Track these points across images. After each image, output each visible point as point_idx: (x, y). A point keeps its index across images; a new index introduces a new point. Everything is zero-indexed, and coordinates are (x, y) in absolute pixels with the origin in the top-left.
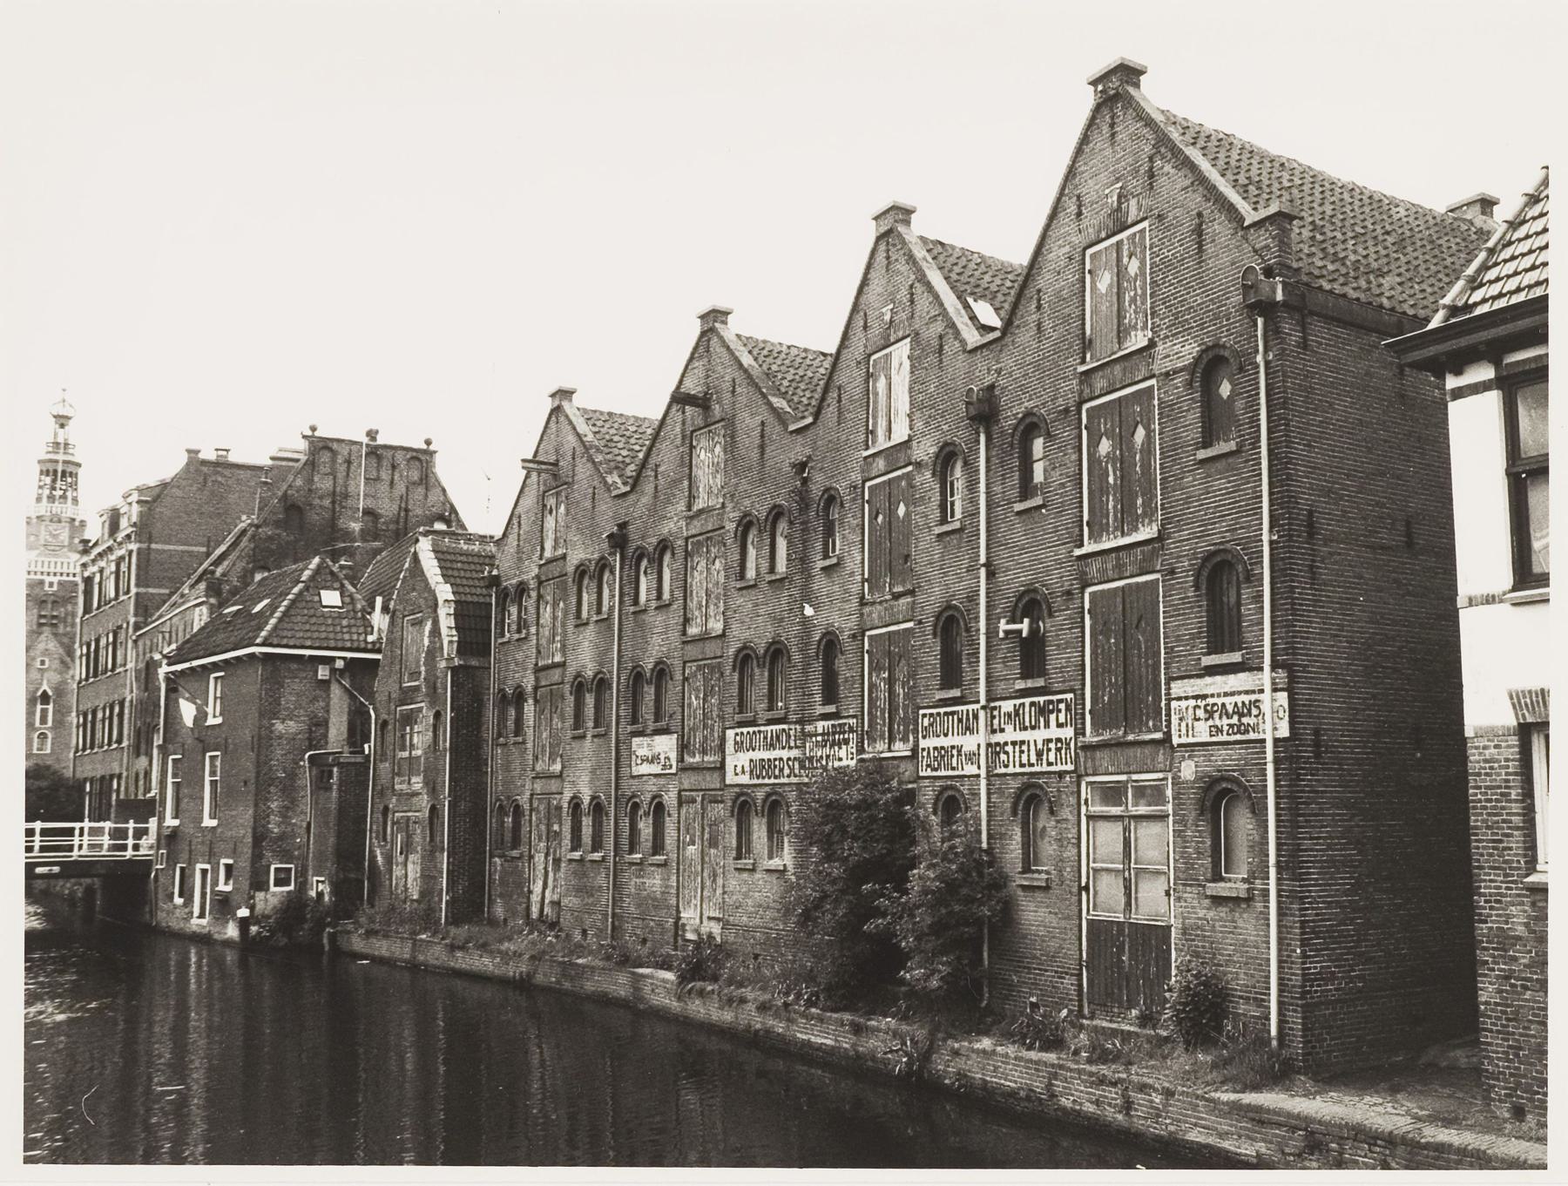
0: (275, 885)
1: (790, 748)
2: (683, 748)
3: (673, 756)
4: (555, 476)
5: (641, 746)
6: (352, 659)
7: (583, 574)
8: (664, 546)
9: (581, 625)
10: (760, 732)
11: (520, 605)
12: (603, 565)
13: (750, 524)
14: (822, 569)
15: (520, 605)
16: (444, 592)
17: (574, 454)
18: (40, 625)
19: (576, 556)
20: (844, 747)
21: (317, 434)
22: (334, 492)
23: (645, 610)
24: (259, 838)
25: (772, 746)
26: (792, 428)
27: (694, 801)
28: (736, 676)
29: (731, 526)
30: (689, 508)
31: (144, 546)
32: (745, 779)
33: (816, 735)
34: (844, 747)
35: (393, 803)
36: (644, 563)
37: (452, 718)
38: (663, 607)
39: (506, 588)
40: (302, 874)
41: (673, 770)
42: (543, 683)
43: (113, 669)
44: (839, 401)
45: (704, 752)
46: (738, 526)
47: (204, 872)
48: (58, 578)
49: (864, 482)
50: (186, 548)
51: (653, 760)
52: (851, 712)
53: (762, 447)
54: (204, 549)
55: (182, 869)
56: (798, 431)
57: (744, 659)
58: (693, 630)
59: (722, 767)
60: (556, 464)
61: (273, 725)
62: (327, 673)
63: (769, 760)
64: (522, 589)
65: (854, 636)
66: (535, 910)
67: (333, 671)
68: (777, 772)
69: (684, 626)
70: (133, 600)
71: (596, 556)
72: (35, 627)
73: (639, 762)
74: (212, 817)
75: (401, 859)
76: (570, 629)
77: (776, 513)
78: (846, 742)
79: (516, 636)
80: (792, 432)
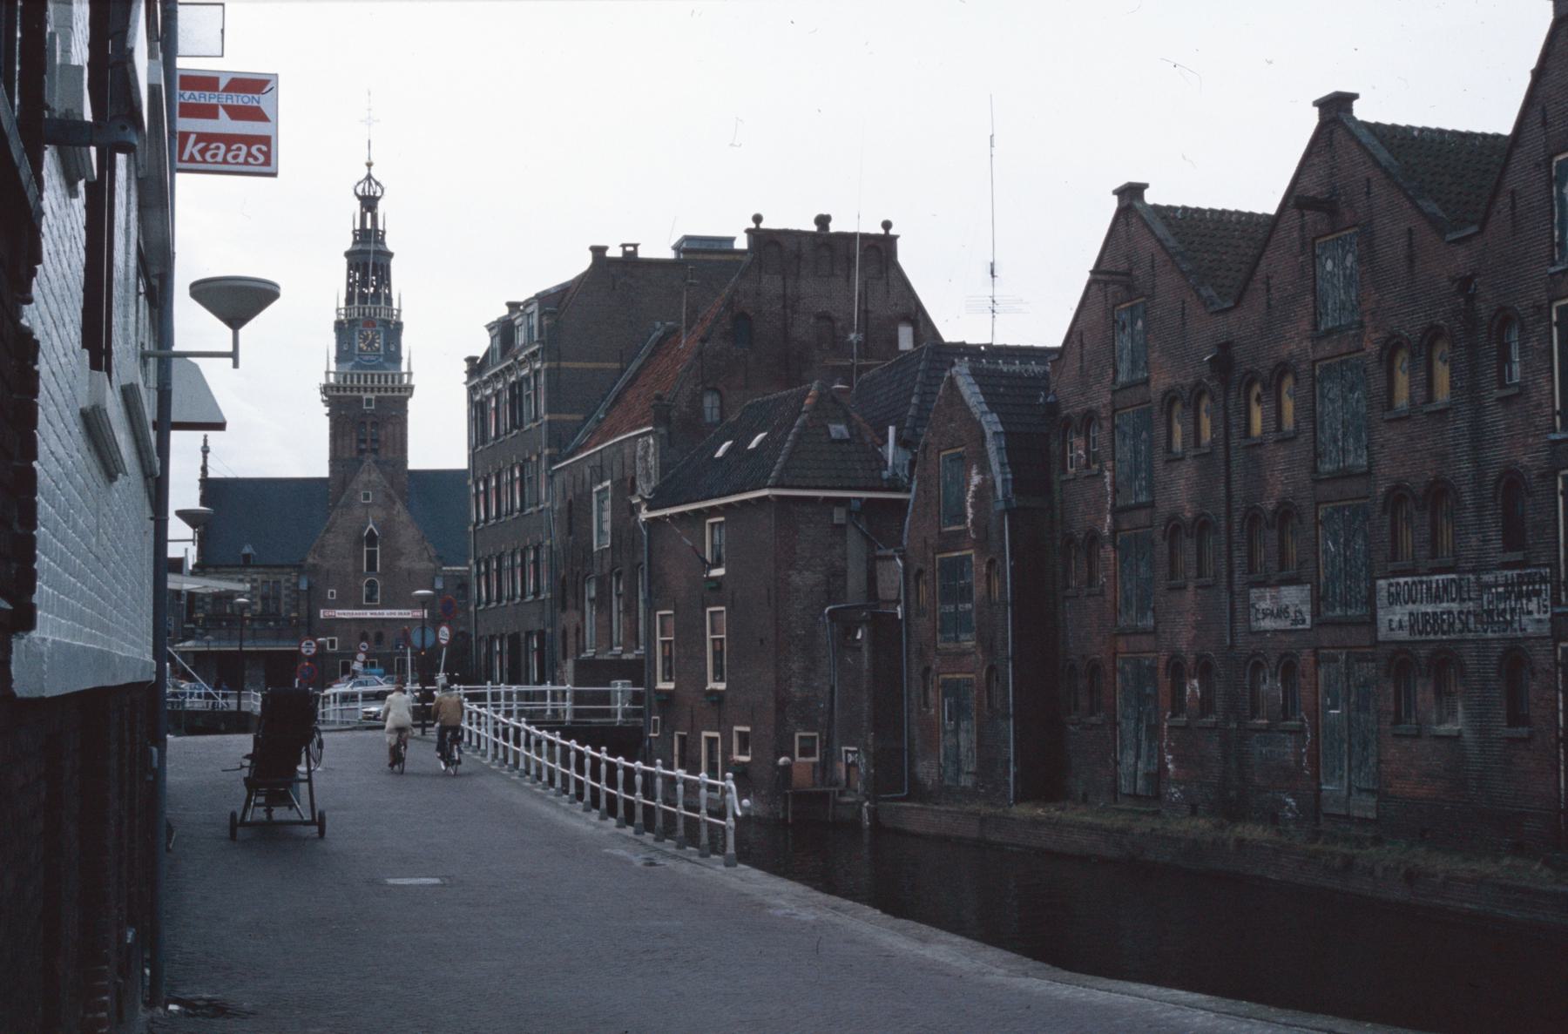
0: (801, 755)
1: (1463, 600)
2: (1317, 600)
3: (1306, 609)
4: (1129, 288)
5: (1264, 600)
6: (869, 500)
7: (1172, 402)
8: (1283, 369)
9: (1172, 459)
10: (1421, 582)
11: (1087, 436)
12: (1198, 392)
13: (1398, 346)
14: (1499, 399)
15: (1087, 436)
16: (991, 424)
17: (1153, 261)
18: (361, 451)
19: (1161, 382)
20: (1535, 600)
21: (763, 226)
22: (785, 295)
23: (1260, 445)
24: (782, 704)
25: (1437, 598)
26: (1449, 237)
27: (1336, 660)
28: (1387, 518)
29: (1372, 348)
30: (1315, 326)
31: (554, 364)
32: (1404, 635)
33: (1496, 586)
34: (1535, 600)
35: (936, 663)
36: (1257, 389)
37: (1011, 568)
38: (1285, 440)
39: (1068, 416)
40: (828, 745)
41: (1307, 626)
42: (1125, 526)
43: (522, 509)
44: (1513, 207)
45: (1347, 605)
46: (1382, 349)
47: (712, 741)
48: (376, 394)
49: (1551, 302)
50: (600, 365)
51: (1281, 613)
52: (1543, 560)
53: (1411, 259)
54: (617, 365)
55: (683, 739)
56: (1458, 241)
57: (1397, 496)
58: (1327, 467)
59: (1373, 621)
60: (1128, 274)
61: (789, 576)
62: (843, 515)
63: (1435, 613)
64: (1089, 418)
65: (1543, 476)
66: (1124, 783)
67: (849, 513)
68: (1445, 627)
69: (1315, 461)
70: (544, 429)
71: (1191, 380)
72: (354, 454)
73: (1260, 616)
74: (668, 676)
75: (950, 725)
76: (1159, 465)
77: (1433, 335)
78: (1538, 594)
79: (1086, 472)
80: (1450, 242)
